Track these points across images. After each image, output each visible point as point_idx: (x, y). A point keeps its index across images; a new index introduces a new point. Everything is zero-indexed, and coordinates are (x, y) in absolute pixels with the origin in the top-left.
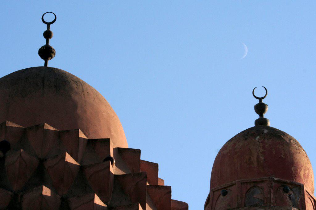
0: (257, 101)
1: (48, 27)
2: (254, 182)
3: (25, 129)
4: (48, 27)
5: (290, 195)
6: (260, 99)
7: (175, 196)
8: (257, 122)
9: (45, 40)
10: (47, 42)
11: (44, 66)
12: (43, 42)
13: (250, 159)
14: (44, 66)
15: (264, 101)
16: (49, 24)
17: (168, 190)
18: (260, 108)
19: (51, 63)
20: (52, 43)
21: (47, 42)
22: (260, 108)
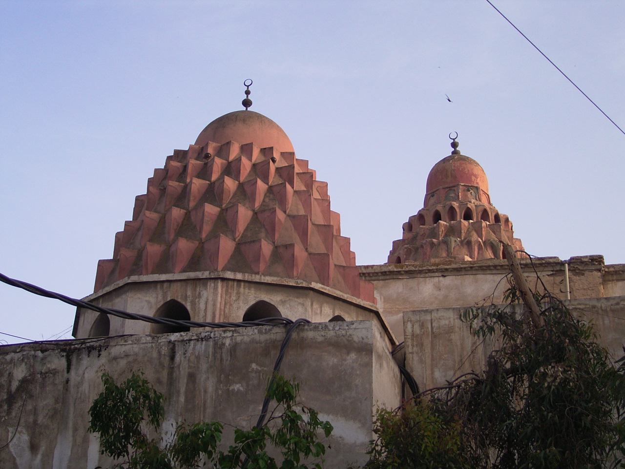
0: (452, 141)
1: (248, 88)
2: (449, 187)
3: (221, 146)
4: (248, 88)
5: (471, 193)
6: (454, 139)
7: (399, 236)
8: (453, 153)
9: (246, 95)
10: (247, 97)
11: (132, 220)
12: (245, 97)
13: (447, 174)
14: (132, 220)
15: (456, 140)
16: (248, 86)
17: (396, 244)
18: (454, 145)
19: (249, 109)
20: (250, 97)
21: (247, 97)
22: (454, 145)
